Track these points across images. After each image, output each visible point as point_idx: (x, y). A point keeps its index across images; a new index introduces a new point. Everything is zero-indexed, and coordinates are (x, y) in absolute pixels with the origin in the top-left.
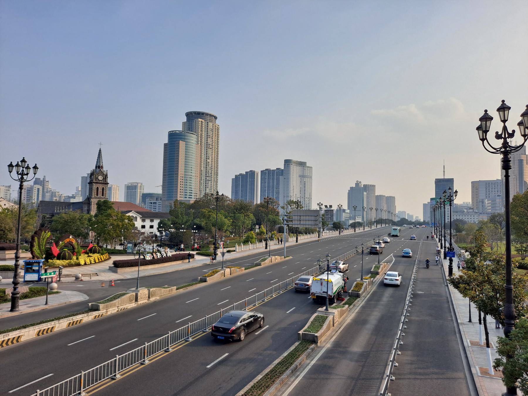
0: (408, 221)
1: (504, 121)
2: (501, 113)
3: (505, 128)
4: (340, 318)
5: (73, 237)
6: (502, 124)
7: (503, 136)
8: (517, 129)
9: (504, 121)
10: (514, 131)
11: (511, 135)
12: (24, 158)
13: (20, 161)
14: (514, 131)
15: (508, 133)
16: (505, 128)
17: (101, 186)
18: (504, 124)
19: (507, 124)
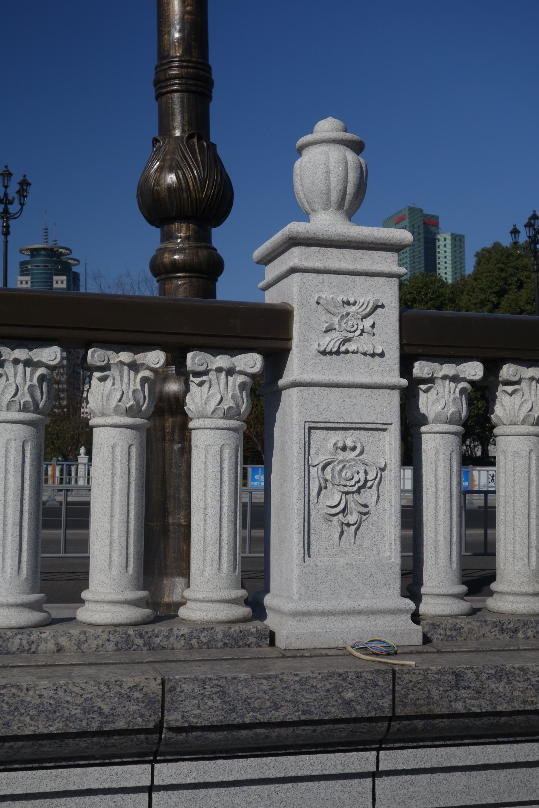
0: (82, 591)
1: (6, 187)
2: (513, 235)
3: (6, 195)
4: (446, 423)
5: (174, 129)
6: (4, 189)
7: (4, 201)
8: (16, 196)
9: (6, 187)
10: (14, 198)
11: (11, 203)
12: (534, 211)
13: (159, 241)
14: (14, 198)
15: (9, 201)
16: (6, 195)
17: (387, 705)
18: (6, 190)
19: (8, 189)
